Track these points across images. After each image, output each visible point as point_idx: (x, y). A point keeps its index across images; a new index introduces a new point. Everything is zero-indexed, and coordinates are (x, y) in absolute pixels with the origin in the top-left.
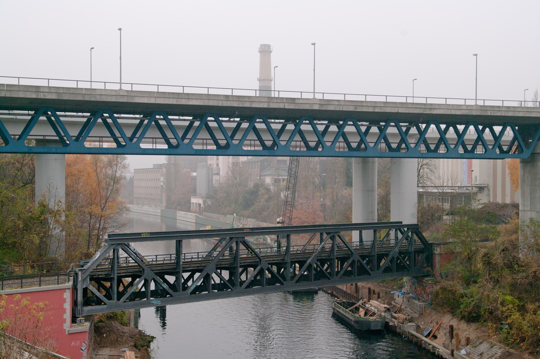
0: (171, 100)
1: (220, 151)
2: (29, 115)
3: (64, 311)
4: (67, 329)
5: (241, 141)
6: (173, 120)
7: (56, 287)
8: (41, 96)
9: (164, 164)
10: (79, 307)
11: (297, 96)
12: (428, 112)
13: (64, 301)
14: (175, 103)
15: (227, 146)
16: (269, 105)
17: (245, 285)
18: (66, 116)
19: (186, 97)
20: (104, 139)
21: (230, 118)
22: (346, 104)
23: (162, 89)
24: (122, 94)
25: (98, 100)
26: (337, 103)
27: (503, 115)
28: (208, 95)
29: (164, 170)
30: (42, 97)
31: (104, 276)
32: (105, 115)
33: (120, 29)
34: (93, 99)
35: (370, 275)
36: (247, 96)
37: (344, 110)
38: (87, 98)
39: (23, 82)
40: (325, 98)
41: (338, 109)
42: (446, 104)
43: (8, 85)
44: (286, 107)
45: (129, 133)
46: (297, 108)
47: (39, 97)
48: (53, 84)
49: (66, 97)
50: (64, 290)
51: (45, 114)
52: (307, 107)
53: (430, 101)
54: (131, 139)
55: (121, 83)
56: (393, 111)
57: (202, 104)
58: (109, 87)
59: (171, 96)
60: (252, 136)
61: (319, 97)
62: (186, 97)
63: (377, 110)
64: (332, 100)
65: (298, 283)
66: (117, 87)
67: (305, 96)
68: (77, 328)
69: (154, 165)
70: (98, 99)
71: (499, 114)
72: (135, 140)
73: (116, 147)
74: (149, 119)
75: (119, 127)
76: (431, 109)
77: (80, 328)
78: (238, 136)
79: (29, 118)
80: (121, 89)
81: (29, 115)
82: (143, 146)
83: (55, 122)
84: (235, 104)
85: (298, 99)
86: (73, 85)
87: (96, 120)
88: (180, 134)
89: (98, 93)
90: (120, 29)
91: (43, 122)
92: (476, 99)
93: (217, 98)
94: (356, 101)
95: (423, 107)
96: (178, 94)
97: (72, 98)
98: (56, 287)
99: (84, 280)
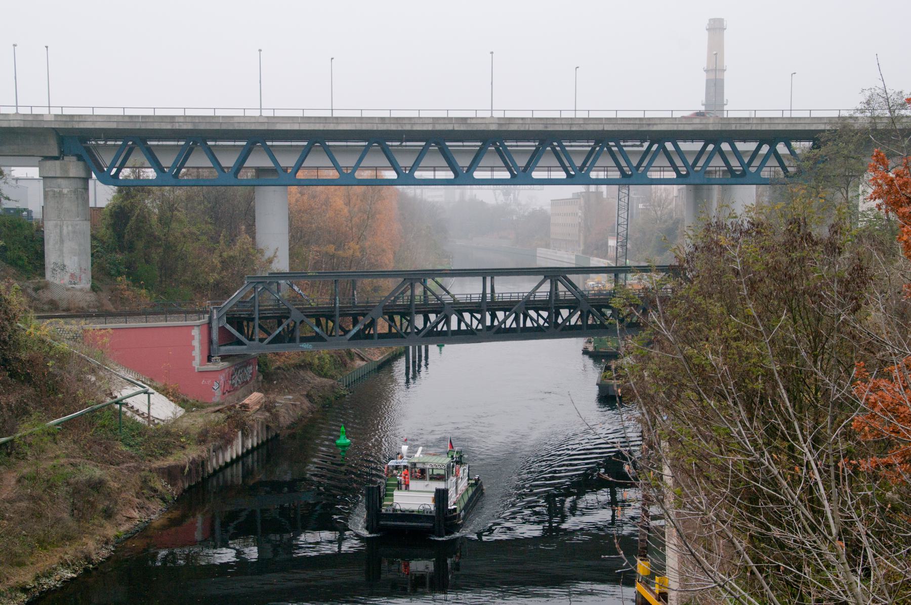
0: (318, 125)
1: (680, 180)
2: (589, 146)
3: (193, 348)
4: (196, 367)
5: (760, 168)
6: (509, 146)
7: (184, 323)
8: (177, 126)
9: (581, 193)
10: (215, 346)
11: (472, 114)
12: (645, 128)
13: (193, 338)
14: (321, 128)
15: (744, 173)
16: (434, 126)
17: (560, 328)
18: (571, 146)
19: (335, 121)
20: (665, 169)
21: (402, 142)
22: (533, 122)
23: (308, 114)
24: (261, 120)
25: (237, 128)
26: (521, 122)
27: (754, 128)
28: (361, 118)
29: (582, 201)
30: (177, 128)
31: (247, 316)
32: (555, 144)
33: (492, 53)
34: (231, 128)
35: (326, 341)
36: (77, 115)
37: (531, 129)
38: (224, 127)
39: (159, 113)
40: (64, 113)
41: (522, 129)
42: (672, 118)
43: (143, 117)
44: (456, 129)
45: (578, 162)
46: (470, 129)
47: (174, 128)
48: (189, 113)
49: (202, 127)
50: (192, 326)
51: (494, 144)
52: (482, 128)
53: (649, 115)
54: (581, 169)
55: (17, 106)
56: (596, 129)
57: (353, 128)
58: (249, 113)
59: (317, 121)
60: (773, 162)
61: (497, 115)
62: (335, 121)
63: (574, 128)
64: (515, 118)
65: (425, 339)
66: (256, 113)
67: (480, 115)
68: (210, 367)
69: (573, 194)
70: (237, 127)
71: (748, 128)
72: (642, 169)
73: (675, 177)
74: (600, 146)
75: (625, 155)
76: (649, 125)
77: (212, 366)
78: (756, 163)
79: (534, 148)
80: (492, 117)
81: (589, 146)
82: (593, 175)
83: (596, 152)
84: (393, 127)
85: (471, 118)
86: (210, 113)
87: (544, 148)
88: (691, 162)
89: (236, 120)
90: (492, 53)
91: (491, 151)
92: (261, 109)
93: (371, 122)
94: (547, 119)
95: (637, 122)
96: (326, 118)
97: (208, 127)
98: (184, 323)
99: (219, 319)
